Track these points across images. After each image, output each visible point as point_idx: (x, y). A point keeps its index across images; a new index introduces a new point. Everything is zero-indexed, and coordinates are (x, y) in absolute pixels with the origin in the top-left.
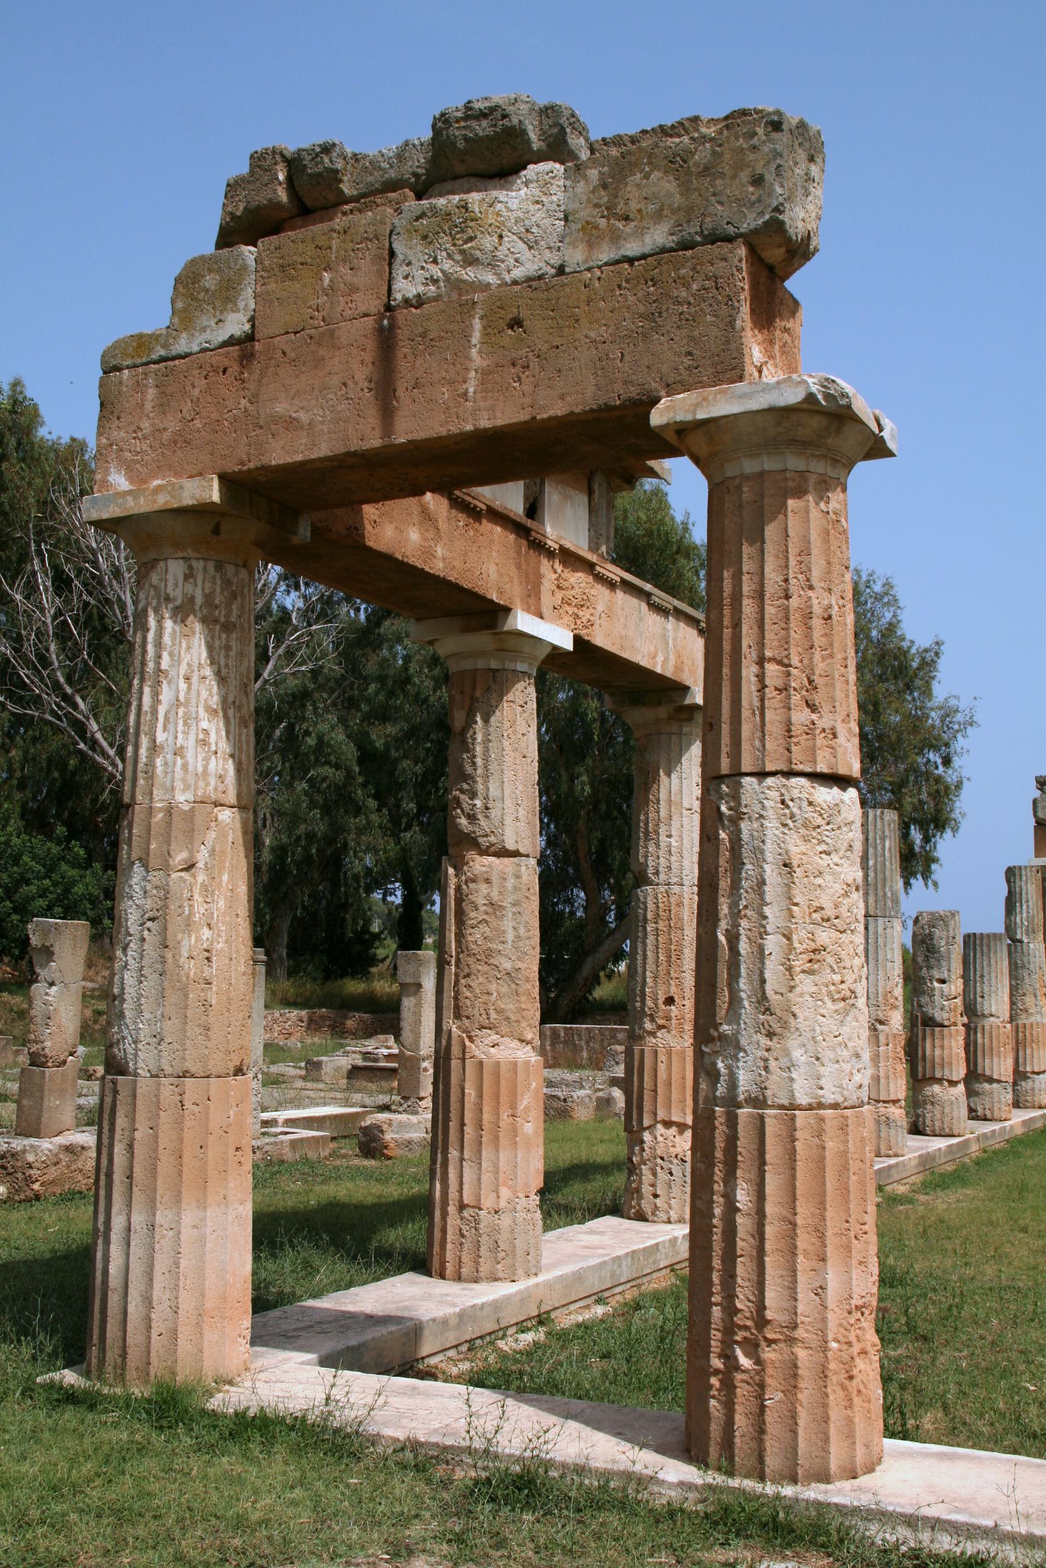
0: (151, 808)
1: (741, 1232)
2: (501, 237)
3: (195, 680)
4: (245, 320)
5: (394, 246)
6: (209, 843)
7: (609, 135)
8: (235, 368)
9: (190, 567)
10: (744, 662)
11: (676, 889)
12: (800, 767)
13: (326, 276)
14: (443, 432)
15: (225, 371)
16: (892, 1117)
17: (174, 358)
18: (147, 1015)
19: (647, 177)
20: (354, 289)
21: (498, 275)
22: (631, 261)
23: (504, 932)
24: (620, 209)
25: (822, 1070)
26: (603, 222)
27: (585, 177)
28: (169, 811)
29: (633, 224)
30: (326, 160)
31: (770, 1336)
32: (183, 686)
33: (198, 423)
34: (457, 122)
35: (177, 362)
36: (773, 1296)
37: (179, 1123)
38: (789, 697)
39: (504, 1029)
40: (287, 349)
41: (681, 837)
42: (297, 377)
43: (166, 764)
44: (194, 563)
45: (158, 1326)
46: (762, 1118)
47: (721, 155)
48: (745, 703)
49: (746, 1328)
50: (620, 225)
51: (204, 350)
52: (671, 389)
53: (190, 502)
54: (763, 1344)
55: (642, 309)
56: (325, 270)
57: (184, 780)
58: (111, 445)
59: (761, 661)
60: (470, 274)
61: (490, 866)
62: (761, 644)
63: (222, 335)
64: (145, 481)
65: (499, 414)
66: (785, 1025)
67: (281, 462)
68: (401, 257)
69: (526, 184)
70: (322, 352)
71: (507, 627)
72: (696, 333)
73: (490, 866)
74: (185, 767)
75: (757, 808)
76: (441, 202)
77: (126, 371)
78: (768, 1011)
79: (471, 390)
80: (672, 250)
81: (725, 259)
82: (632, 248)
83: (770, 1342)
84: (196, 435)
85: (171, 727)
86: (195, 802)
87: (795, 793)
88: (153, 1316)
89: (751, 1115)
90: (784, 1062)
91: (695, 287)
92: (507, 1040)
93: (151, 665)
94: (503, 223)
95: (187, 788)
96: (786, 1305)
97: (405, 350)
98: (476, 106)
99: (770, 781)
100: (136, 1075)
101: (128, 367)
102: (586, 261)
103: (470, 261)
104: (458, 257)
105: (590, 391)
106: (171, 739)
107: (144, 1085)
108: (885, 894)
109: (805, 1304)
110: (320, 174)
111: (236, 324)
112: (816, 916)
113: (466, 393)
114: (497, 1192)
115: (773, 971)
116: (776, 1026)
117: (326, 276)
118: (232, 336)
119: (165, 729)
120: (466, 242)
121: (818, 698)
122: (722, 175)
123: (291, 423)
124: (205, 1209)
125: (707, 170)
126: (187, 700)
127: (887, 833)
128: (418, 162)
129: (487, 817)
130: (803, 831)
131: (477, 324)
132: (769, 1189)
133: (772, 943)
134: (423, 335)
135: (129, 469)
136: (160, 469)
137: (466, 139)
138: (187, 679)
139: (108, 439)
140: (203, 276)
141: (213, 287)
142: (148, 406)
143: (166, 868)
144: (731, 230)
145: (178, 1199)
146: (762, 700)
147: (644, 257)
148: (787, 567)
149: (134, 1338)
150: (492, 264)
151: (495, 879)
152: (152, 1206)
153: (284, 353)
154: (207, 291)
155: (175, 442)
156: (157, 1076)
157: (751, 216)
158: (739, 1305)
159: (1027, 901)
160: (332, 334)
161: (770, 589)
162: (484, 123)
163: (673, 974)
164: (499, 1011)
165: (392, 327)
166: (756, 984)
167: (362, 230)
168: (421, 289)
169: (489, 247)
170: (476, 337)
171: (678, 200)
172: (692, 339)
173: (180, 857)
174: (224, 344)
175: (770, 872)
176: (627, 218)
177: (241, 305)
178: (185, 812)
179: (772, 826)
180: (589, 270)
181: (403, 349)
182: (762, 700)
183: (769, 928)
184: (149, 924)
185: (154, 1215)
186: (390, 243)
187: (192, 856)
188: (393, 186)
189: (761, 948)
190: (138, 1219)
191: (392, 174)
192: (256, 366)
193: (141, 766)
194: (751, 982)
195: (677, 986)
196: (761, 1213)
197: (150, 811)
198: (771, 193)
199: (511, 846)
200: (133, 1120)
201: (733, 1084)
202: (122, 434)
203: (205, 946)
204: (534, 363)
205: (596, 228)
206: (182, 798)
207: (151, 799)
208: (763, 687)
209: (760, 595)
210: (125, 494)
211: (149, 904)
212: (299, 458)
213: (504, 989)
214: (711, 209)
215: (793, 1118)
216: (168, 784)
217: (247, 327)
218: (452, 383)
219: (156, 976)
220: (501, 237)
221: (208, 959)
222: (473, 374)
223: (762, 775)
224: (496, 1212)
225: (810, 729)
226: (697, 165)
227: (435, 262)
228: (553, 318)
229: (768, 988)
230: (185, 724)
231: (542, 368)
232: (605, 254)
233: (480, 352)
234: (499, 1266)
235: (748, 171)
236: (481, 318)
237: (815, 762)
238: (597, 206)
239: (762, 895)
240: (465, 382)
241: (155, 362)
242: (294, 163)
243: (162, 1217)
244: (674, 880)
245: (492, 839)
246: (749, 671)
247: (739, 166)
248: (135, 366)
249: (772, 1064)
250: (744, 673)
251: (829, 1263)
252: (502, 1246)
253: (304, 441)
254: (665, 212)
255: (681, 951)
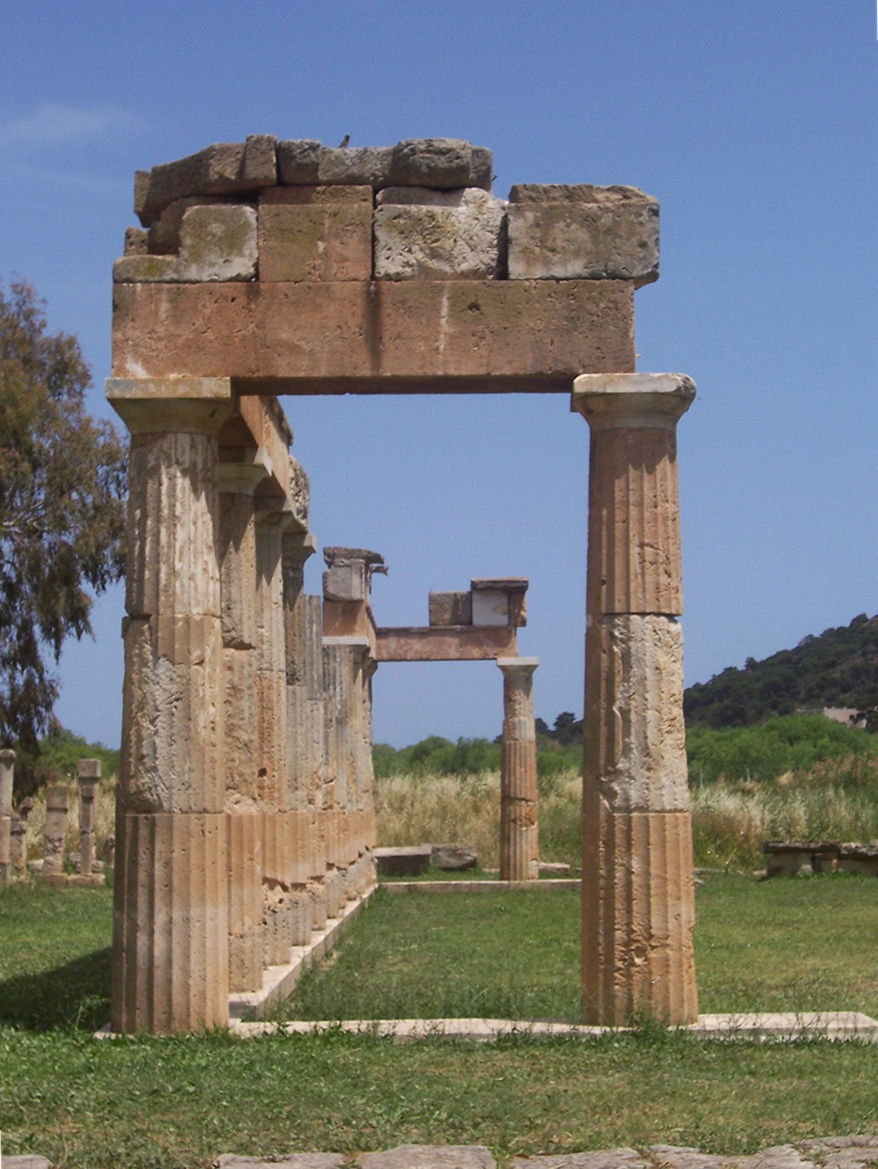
0: (174, 618)
1: (635, 886)
2: (455, 241)
3: (200, 524)
4: (251, 264)
5: (377, 233)
6: (211, 645)
7: (529, 183)
8: (242, 300)
9: (193, 440)
10: (631, 545)
11: (267, 674)
12: (663, 610)
13: (321, 246)
14: (420, 373)
15: (233, 300)
16: (317, 893)
17: (185, 282)
18: (178, 769)
19: (568, 226)
20: (345, 259)
21: (452, 267)
22: (558, 280)
23: (243, 710)
24: (549, 243)
25: (676, 790)
26: (537, 250)
27: (523, 216)
28: (188, 620)
29: (559, 256)
30: (313, 155)
31: (653, 944)
32: (193, 529)
33: (210, 335)
34: (422, 152)
35: (187, 285)
36: (655, 921)
37: (202, 845)
38: (658, 568)
39: (244, 789)
40: (289, 292)
41: (270, 627)
42: (299, 315)
43: (182, 586)
44: (195, 437)
45: (193, 990)
46: (646, 818)
47: (619, 223)
48: (632, 570)
49: (638, 941)
50: (550, 254)
51: (213, 281)
52: (587, 369)
53: (209, 395)
54: (649, 949)
55: (566, 313)
56: (319, 239)
57: (196, 598)
58: (127, 340)
59: (642, 545)
60: (434, 264)
61: (232, 656)
62: (641, 534)
63: (231, 272)
64: (161, 373)
65: (463, 367)
66: (658, 763)
67: (287, 375)
68: (383, 243)
69: (467, 203)
70: (319, 300)
71: (255, 462)
72: (603, 336)
73: (232, 656)
74: (196, 588)
75: (640, 634)
76: (413, 208)
77: (139, 285)
78: (648, 755)
79: (442, 347)
80: (585, 278)
81: (622, 291)
82: (558, 271)
83: (653, 947)
84: (209, 345)
85: (186, 559)
86: (205, 614)
87: (661, 626)
88: (191, 982)
89: (639, 817)
90: (658, 785)
91: (602, 305)
92: (245, 798)
93: (165, 512)
94: (457, 231)
95: (198, 604)
96: (663, 925)
97: (389, 311)
98: (436, 144)
99: (647, 618)
100: (170, 811)
101: (140, 281)
102: (525, 274)
103: (434, 254)
104: (428, 252)
105: (529, 362)
106: (186, 568)
107: (178, 818)
108: (312, 676)
109: (672, 924)
110: (307, 165)
111: (242, 266)
112: (672, 699)
113: (437, 349)
114: (242, 920)
115: (651, 732)
116: (653, 764)
117: (321, 246)
118: (238, 275)
119: (180, 560)
120: (434, 242)
121: (671, 568)
122: (620, 237)
123: (294, 349)
124: (217, 907)
125: (609, 231)
126: (196, 539)
127: (314, 618)
128: (375, 167)
129: (229, 616)
130: (665, 649)
131: (445, 303)
132: (652, 859)
133: (650, 714)
134: (403, 302)
135: (147, 362)
136: (175, 366)
137: (428, 166)
138: (195, 523)
139: (124, 335)
140: (210, 224)
141: (219, 234)
142: (163, 315)
143: (187, 662)
144: (626, 273)
145: (203, 899)
146: (643, 568)
147: (566, 279)
148: (655, 488)
149: (177, 997)
150: (449, 259)
151: (236, 667)
152: (187, 907)
153: (286, 295)
154: (214, 236)
155: (189, 347)
156: (187, 812)
157: (639, 267)
158: (634, 928)
159: (341, 683)
160: (328, 288)
161: (647, 501)
162: (443, 159)
163: (266, 749)
164: (241, 775)
165: (378, 293)
166: (642, 739)
167: (350, 217)
168: (400, 269)
169: (448, 248)
170: (445, 311)
171: (590, 246)
172: (600, 339)
173: (196, 654)
174: (231, 280)
175: (649, 672)
176: (553, 250)
177: (247, 252)
178: (197, 622)
179: (649, 644)
180: (527, 280)
181: (387, 309)
182: (643, 568)
183: (649, 706)
184: (175, 703)
185: (189, 911)
186: (373, 232)
187: (203, 654)
188: (354, 180)
189: (644, 718)
190: (177, 915)
191: (355, 170)
192: (263, 302)
193: (161, 586)
194: (637, 738)
195: (269, 759)
196: (648, 874)
197: (173, 620)
198: (652, 255)
199: (246, 640)
200: (171, 844)
201: (627, 799)
202: (137, 333)
203: (211, 719)
204: (488, 336)
205: (532, 252)
206: (196, 611)
207: (173, 612)
208: (643, 561)
209: (640, 504)
210: (145, 381)
211: (174, 688)
212: (302, 374)
213: (243, 757)
214: (613, 257)
215: (664, 817)
216: (185, 601)
217: (252, 270)
218: (426, 340)
219: (182, 740)
220: (455, 241)
221: (213, 729)
222: (442, 336)
223: (643, 614)
224: (242, 937)
225: (668, 587)
226: (603, 225)
227: (410, 251)
228: (502, 308)
229: (649, 741)
230: (195, 557)
231: (495, 341)
232: (539, 272)
233: (447, 321)
234: (244, 980)
235: (638, 237)
236: (449, 298)
237: (670, 607)
238: (533, 238)
239: (644, 686)
240: (437, 341)
241: (167, 282)
242: (283, 153)
243: (194, 913)
244: (266, 666)
245: (233, 634)
246: (634, 551)
247: (631, 233)
248: (147, 282)
249: (652, 786)
250: (631, 551)
251: (683, 900)
252: (247, 964)
253: (306, 363)
254: (582, 252)
255: (272, 729)
